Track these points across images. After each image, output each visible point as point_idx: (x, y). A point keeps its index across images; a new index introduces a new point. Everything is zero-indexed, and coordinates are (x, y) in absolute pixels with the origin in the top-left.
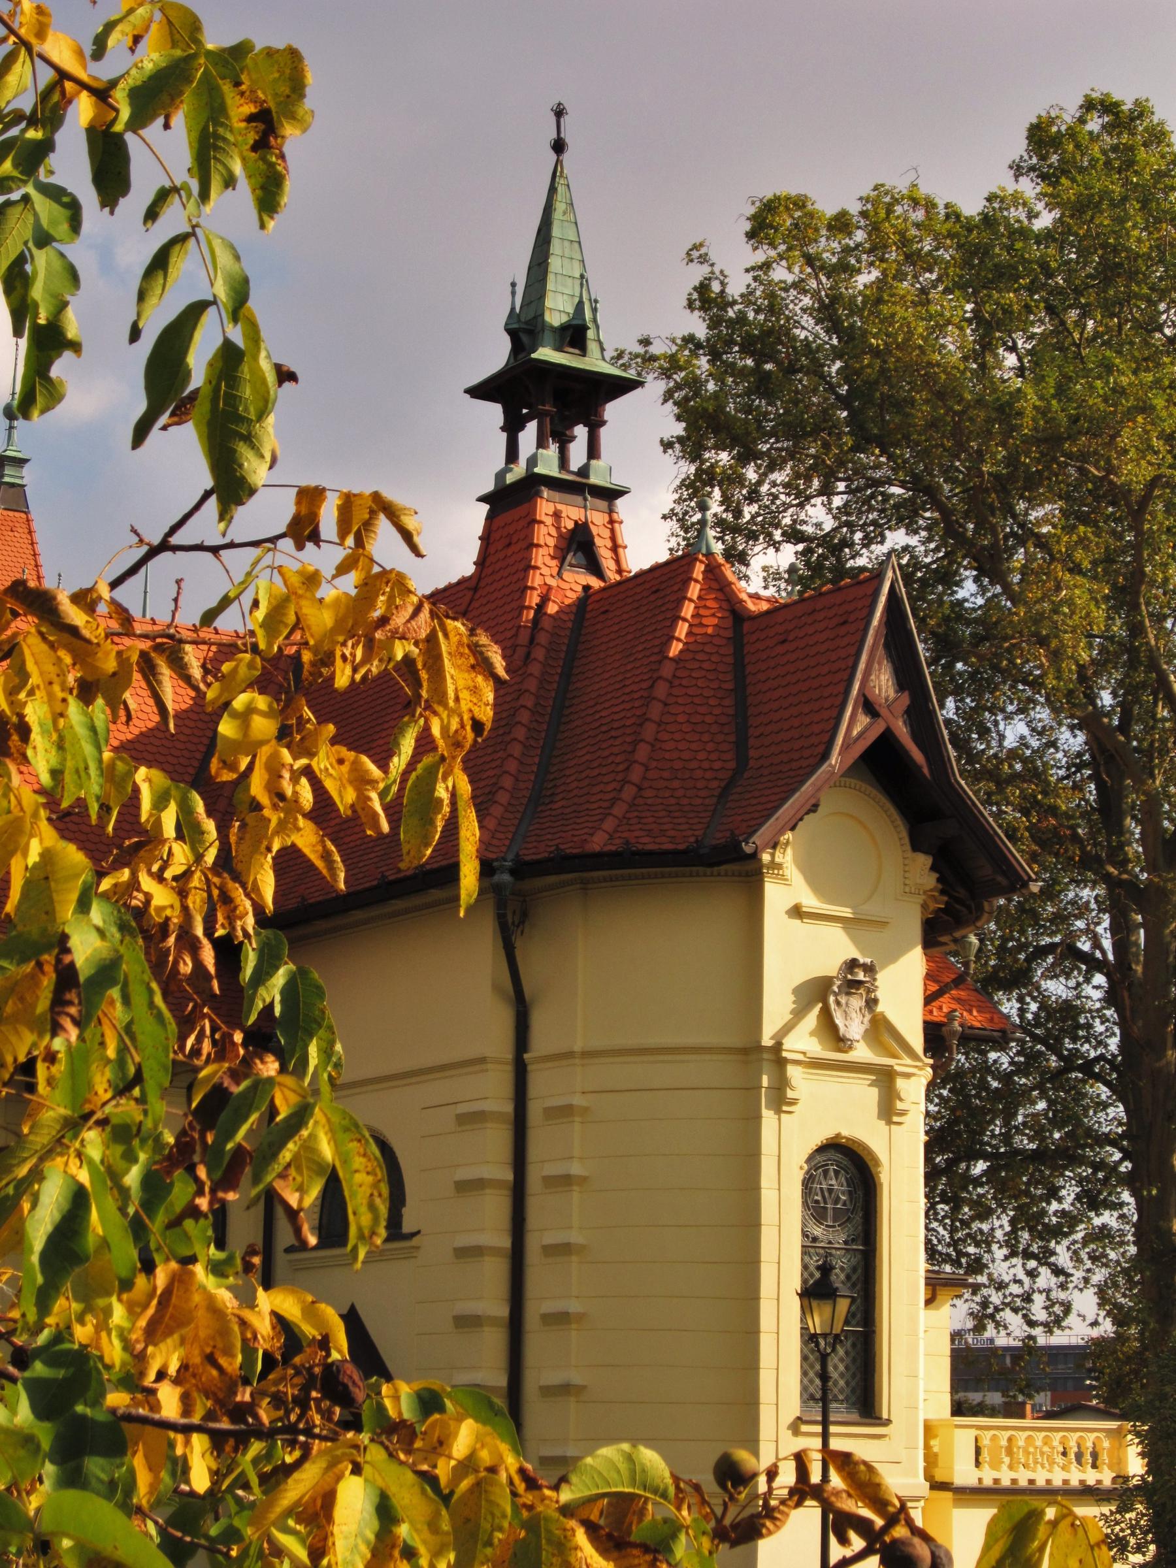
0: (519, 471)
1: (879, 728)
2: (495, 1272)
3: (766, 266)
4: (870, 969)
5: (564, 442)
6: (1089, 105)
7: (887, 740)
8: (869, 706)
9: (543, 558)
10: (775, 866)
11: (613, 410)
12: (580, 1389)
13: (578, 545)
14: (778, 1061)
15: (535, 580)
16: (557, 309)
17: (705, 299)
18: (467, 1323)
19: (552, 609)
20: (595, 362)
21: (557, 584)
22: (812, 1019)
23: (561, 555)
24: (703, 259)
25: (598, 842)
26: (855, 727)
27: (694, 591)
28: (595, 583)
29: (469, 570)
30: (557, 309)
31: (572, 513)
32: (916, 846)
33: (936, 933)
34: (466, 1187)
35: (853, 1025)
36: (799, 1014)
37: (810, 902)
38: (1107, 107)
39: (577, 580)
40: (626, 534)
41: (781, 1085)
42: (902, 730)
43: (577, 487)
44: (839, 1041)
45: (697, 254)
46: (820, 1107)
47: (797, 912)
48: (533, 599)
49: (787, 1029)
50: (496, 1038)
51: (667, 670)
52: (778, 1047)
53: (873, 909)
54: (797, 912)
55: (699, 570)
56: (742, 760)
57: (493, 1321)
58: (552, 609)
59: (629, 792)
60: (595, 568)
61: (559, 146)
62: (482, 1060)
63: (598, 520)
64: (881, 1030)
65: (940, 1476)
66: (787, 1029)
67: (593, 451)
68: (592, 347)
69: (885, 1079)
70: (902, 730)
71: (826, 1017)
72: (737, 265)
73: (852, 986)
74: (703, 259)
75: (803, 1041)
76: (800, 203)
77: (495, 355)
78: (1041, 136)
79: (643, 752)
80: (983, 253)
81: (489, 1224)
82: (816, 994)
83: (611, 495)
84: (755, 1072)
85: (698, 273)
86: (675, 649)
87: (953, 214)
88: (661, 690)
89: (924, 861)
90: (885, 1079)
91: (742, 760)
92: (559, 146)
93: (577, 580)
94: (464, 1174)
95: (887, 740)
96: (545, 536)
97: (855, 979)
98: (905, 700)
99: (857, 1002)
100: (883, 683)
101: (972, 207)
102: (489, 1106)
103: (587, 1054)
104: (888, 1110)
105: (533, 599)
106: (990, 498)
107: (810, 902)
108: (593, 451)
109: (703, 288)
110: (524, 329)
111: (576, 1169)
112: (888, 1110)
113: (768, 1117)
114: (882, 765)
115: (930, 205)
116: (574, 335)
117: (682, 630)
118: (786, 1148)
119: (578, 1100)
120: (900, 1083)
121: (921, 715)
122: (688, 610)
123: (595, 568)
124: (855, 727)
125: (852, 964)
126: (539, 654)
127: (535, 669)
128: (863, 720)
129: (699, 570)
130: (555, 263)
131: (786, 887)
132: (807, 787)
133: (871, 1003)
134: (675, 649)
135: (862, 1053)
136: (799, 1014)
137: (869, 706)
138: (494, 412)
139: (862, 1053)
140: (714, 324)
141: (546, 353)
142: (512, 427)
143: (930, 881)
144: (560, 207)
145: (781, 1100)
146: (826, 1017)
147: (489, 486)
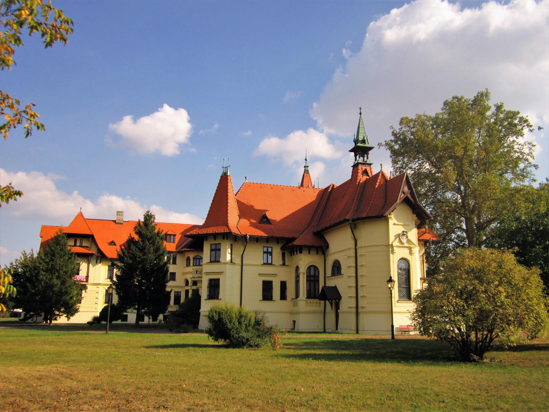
0: (357, 162)
1: (406, 196)
2: (353, 279)
3: (402, 128)
4: (406, 232)
5: (364, 157)
6: (453, 98)
7: (407, 198)
8: (404, 193)
9: (360, 175)
10: (390, 217)
11: (370, 152)
12: (366, 296)
13: (365, 172)
14: (393, 247)
15: (359, 178)
16: (361, 138)
17: (394, 134)
18: (350, 287)
19: (361, 182)
20: (367, 145)
21: (362, 178)
22: (398, 239)
23: (363, 174)
24: (393, 128)
25: (364, 216)
26: (401, 196)
27: (380, 178)
28: (368, 177)
29: (350, 178)
30: (361, 138)
31: (364, 168)
32: (413, 213)
33: (419, 227)
34: (349, 267)
35: (404, 240)
36: (395, 239)
37: (396, 222)
38: (457, 98)
39: (365, 177)
40: (373, 170)
41: (393, 250)
42: (409, 196)
43: (364, 164)
44: (402, 243)
45: (392, 127)
46: (399, 253)
47: (394, 224)
48: (358, 181)
49: (394, 242)
50: (352, 245)
51: (375, 190)
52: (392, 244)
53: (407, 223)
54: (394, 224)
55: (380, 175)
56: (386, 202)
57: (353, 287)
58: (361, 182)
59: (369, 208)
60: (368, 175)
61: (360, 114)
62: (350, 249)
63: (368, 168)
64: (409, 241)
65: (323, 331)
66: (394, 242)
67: (367, 158)
68: (367, 143)
69: (410, 249)
70: (409, 196)
71: (400, 239)
72: (397, 128)
73: (404, 235)
74: (393, 128)
75: (396, 243)
76: (407, 118)
77: (353, 145)
78: (446, 104)
79: (371, 202)
80: (436, 121)
81: (352, 272)
82: (398, 236)
83: (370, 164)
84: (388, 248)
85: (392, 130)
86: (377, 186)
87: (430, 117)
88: (374, 193)
89: (415, 215)
90: (410, 249)
91: (386, 202)
92: (360, 114)
93: (365, 177)
94: (349, 265)
95: (407, 198)
96: (360, 171)
97: (404, 234)
98: (410, 191)
99: (405, 237)
100: (406, 189)
101: (433, 115)
102: (351, 255)
103: (364, 247)
104: (411, 253)
105: (358, 181)
106: (440, 159)
107: (396, 222)
108: (367, 158)
109: (393, 132)
110: (356, 141)
111: (364, 264)
112: (411, 253)
113: (391, 255)
114: (406, 201)
115: (427, 116)
116: (363, 141)
117: (378, 184)
118: (394, 259)
119: (364, 254)
120: (412, 249)
121: (412, 193)
122: (379, 180)
123: (368, 175)
124: (401, 196)
125: (403, 232)
126: (359, 189)
127: (358, 191)
128: (403, 195)
129: (380, 175)
130: (360, 131)
131: (393, 220)
132: (394, 206)
133: (407, 237)
134: (377, 186)
135: (406, 245)
136: (395, 239)
137: (404, 193)
138: (353, 154)
139: (406, 245)
140: (396, 137)
141: (359, 144)
142: (356, 156)
143: (416, 218)
144: (361, 123)
145: (393, 252)
146: (400, 239)
147: (353, 165)
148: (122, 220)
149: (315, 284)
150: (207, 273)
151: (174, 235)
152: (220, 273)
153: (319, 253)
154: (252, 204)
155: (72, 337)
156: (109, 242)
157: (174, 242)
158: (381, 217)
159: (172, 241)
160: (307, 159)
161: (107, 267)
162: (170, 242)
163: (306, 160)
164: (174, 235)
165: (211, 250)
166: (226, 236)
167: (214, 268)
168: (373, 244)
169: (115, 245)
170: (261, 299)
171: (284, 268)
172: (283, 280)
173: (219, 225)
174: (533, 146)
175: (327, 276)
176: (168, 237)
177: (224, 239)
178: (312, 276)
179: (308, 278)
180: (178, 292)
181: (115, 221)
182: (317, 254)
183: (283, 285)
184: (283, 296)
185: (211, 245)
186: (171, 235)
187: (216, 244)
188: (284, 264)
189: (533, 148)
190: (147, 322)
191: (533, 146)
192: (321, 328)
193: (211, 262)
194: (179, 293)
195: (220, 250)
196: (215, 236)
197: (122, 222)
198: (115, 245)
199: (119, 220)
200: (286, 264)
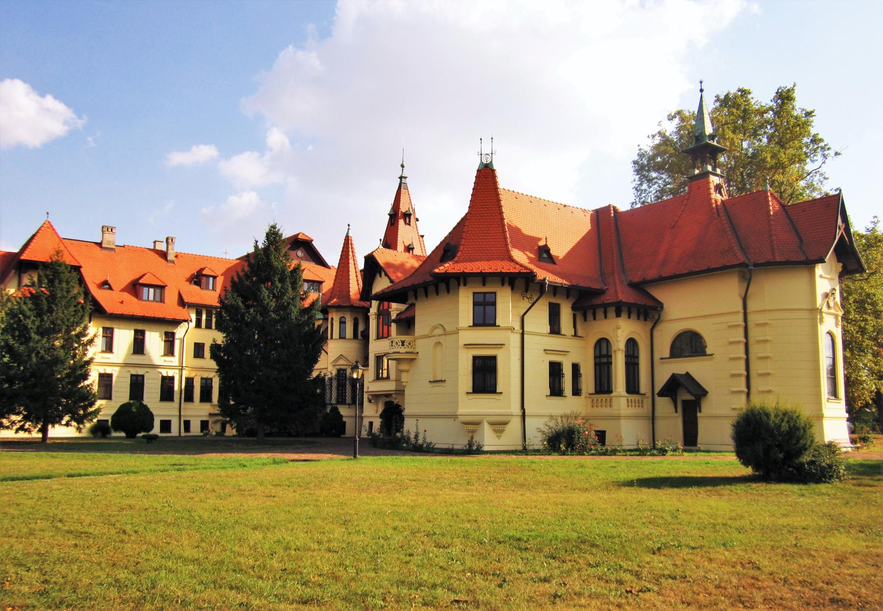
14: (821, 312)
48: (714, 205)
54: (821, 276)
91: (801, 241)
145: (821, 321)
148: (113, 244)
149: (634, 369)
150: (467, 346)
151: (215, 277)
152: (500, 346)
153: (632, 316)
154: (519, 226)
155: (55, 462)
156: (98, 282)
157: (214, 289)
158: (809, 263)
159: (211, 287)
160: (405, 164)
161: (133, 332)
162: (207, 288)
163: (402, 166)
164: (215, 277)
165: (475, 304)
166: (507, 279)
167: (484, 335)
168: (784, 307)
169: (111, 288)
170: (549, 393)
171: (575, 342)
172: (576, 361)
173: (494, 259)
174: (825, 178)
175: (657, 357)
176: (204, 280)
177: (503, 285)
178: (604, 356)
179: (598, 360)
180: (206, 379)
181: (100, 245)
182: (629, 317)
183: (576, 368)
184: (576, 392)
185: (474, 293)
186: (208, 276)
187: (485, 293)
188: (575, 335)
189: (825, 182)
190: (177, 434)
191: (825, 178)
192: (645, 443)
193: (475, 325)
194: (209, 381)
195: (494, 304)
196: (484, 278)
197: (113, 247)
198: (111, 288)
199: (109, 242)
200: (579, 333)
